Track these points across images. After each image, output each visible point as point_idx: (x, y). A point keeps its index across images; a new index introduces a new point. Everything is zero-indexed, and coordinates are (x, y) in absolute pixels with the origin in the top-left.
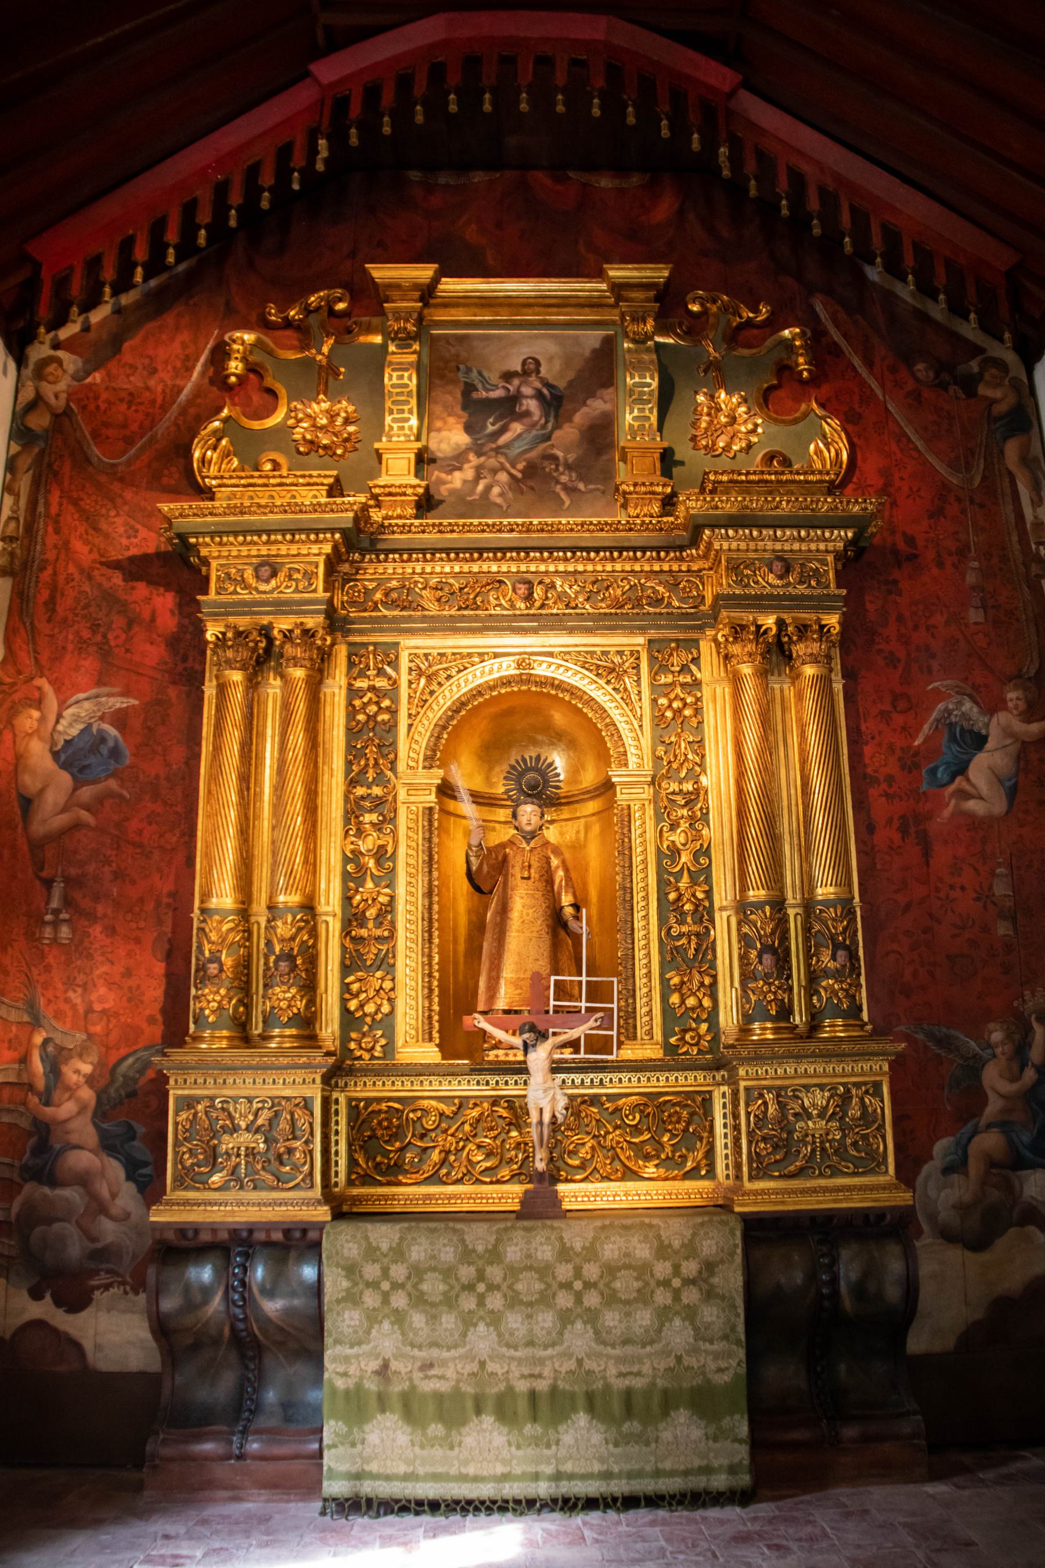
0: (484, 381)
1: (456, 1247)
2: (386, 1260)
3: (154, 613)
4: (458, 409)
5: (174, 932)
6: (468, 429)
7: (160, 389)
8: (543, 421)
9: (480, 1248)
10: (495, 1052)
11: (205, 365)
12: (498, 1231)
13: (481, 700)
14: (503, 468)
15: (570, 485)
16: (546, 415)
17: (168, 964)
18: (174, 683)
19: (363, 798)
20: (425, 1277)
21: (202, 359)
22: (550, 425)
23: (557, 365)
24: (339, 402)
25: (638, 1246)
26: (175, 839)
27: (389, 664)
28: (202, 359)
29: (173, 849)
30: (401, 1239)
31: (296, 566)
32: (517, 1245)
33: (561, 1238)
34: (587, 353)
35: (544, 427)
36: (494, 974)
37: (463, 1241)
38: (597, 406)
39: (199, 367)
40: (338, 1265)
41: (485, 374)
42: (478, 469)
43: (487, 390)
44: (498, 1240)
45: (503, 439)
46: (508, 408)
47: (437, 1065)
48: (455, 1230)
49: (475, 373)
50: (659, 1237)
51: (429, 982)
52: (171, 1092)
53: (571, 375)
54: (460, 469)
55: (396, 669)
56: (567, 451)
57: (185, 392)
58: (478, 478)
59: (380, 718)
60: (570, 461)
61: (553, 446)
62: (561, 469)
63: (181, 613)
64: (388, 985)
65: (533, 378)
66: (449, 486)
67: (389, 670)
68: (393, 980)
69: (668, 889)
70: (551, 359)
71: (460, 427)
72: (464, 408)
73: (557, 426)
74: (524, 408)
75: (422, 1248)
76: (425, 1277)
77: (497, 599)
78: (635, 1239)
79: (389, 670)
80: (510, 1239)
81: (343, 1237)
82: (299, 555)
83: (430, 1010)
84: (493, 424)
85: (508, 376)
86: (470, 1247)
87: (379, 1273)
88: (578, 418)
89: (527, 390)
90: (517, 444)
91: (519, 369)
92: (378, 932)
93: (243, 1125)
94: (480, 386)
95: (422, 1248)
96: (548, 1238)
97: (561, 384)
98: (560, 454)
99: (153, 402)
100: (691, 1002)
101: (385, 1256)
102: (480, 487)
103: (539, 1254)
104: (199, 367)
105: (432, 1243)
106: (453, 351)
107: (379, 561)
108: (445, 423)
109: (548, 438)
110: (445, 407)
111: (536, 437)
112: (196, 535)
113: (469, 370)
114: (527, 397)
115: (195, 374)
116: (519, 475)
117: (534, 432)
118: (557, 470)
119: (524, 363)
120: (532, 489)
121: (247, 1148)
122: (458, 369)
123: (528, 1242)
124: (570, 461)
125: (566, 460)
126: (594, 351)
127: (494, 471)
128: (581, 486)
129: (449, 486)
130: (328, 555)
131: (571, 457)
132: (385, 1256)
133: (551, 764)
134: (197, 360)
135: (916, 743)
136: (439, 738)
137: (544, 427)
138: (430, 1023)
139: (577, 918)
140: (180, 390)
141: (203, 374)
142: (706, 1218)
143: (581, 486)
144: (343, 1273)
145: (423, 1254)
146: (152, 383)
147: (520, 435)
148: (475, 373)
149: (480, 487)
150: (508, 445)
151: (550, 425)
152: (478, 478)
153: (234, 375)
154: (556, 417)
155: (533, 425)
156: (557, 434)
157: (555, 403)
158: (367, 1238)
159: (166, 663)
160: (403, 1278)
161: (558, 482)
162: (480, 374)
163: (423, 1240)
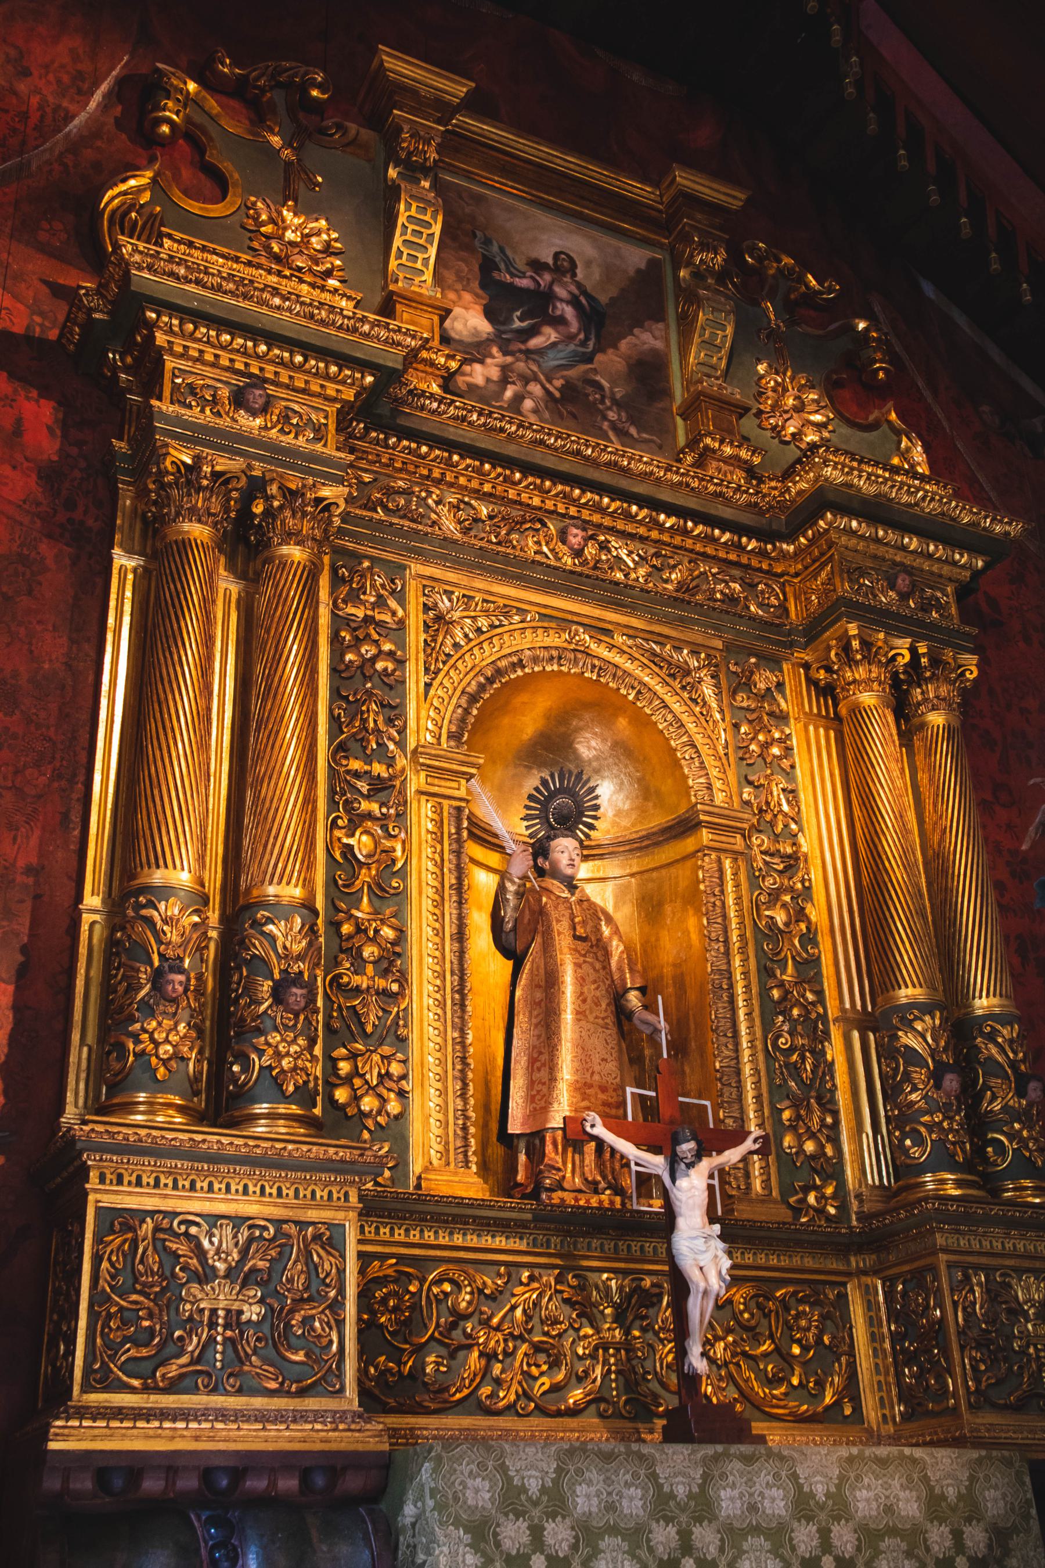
0: (509, 263)
1: (646, 1490)
2: (536, 1513)
3: (19, 421)
4: (475, 285)
5: (32, 935)
6: (489, 314)
7: (35, 100)
8: (582, 336)
9: (681, 1491)
10: (560, 1193)
11: (107, 96)
12: (705, 1461)
13: (520, 673)
14: (536, 379)
15: (620, 426)
16: (585, 327)
17: (18, 989)
18: (49, 536)
19: (357, 775)
20: (602, 1545)
21: (104, 87)
22: (591, 344)
23: (597, 274)
24: (317, 220)
25: (902, 1495)
26: (43, 780)
27: (393, 592)
28: (104, 87)
29: (40, 797)
30: (559, 1470)
31: (296, 407)
32: (733, 1486)
33: (794, 1476)
34: (631, 272)
35: (584, 344)
36: (544, 1074)
37: (654, 1476)
38: (648, 339)
39: (98, 97)
40: (457, 1523)
41: (509, 253)
42: (505, 369)
43: (512, 275)
44: (706, 1477)
45: (535, 342)
46: (539, 306)
47: (482, 1204)
48: (641, 1457)
49: (495, 248)
50: (925, 1479)
51: (462, 1071)
52: (91, 1198)
53: (613, 292)
54: (481, 362)
55: (402, 602)
56: (613, 382)
57: (76, 121)
58: (504, 381)
59: (380, 666)
60: (618, 396)
61: (595, 371)
62: (608, 402)
63: (65, 436)
64: (395, 1069)
65: (567, 279)
66: (468, 379)
67: (392, 604)
68: (404, 1062)
69: (771, 983)
70: (588, 263)
71: (479, 308)
72: (483, 286)
73: (600, 349)
74: (558, 313)
75: (593, 1490)
76: (602, 1545)
77: (538, 543)
78: (896, 1483)
79: (392, 604)
80: (723, 1476)
81: (465, 1468)
82: (303, 391)
83: (467, 1118)
84: (521, 319)
85: (537, 266)
86: (666, 1489)
87: (525, 1539)
88: (624, 345)
89: (560, 291)
90: (551, 354)
91: (550, 261)
92: (381, 983)
93: (221, 1266)
94: (502, 266)
95: (593, 1490)
96: (777, 1476)
97: (603, 298)
98: (606, 384)
99: (25, 116)
100: (810, 1147)
101: (536, 1504)
102: (509, 394)
103: (767, 1503)
104: (98, 97)
105: (608, 1481)
106: (467, 210)
107: (387, 446)
108: (460, 297)
109: (589, 359)
110: (460, 278)
111: (575, 354)
112: (165, 306)
113: (487, 242)
114: (562, 300)
115: (93, 105)
116: (557, 394)
117: (572, 347)
118: (602, 402)
119: (556, 255)
120: (575, 417)
121: (228, 1311)
122: (475, 236)
123: (750, 1483)
124: (618, 396)
125: (613, 393)
126: (639, 271)
127: (526, 380)
128: (633, 431)
129: (468, 379)
130: (345, 402)
131: (619, 392)
132: (536, 1504)
133: (593, 789)
134: (96, 85)
135: (1024, 848)
136: (467, 711)
137: (584, 344)
138: (465, 1138)
139: (650, 1007)
140: (69, 118)
141: (105, 106)
142: (983, 1453)
143: (633, 431)
144: (467, 1538)
145: (595, 1501)
146: (22, 87)
147: (554, 345)
148: (495, 248)
149: (509, 394)
150: (540, 352)
151: (591, 344)
152: (504, 381)
153: (169, 121)
154: (598, 338)
155: (571, 338)
156: (599, 357)
157: (599, 322)
158: (503, 1469)
159: (38, 504)
160: (565, 1546)
161: (605, 418)
162: (502, 250)
163: (593, 1475)
